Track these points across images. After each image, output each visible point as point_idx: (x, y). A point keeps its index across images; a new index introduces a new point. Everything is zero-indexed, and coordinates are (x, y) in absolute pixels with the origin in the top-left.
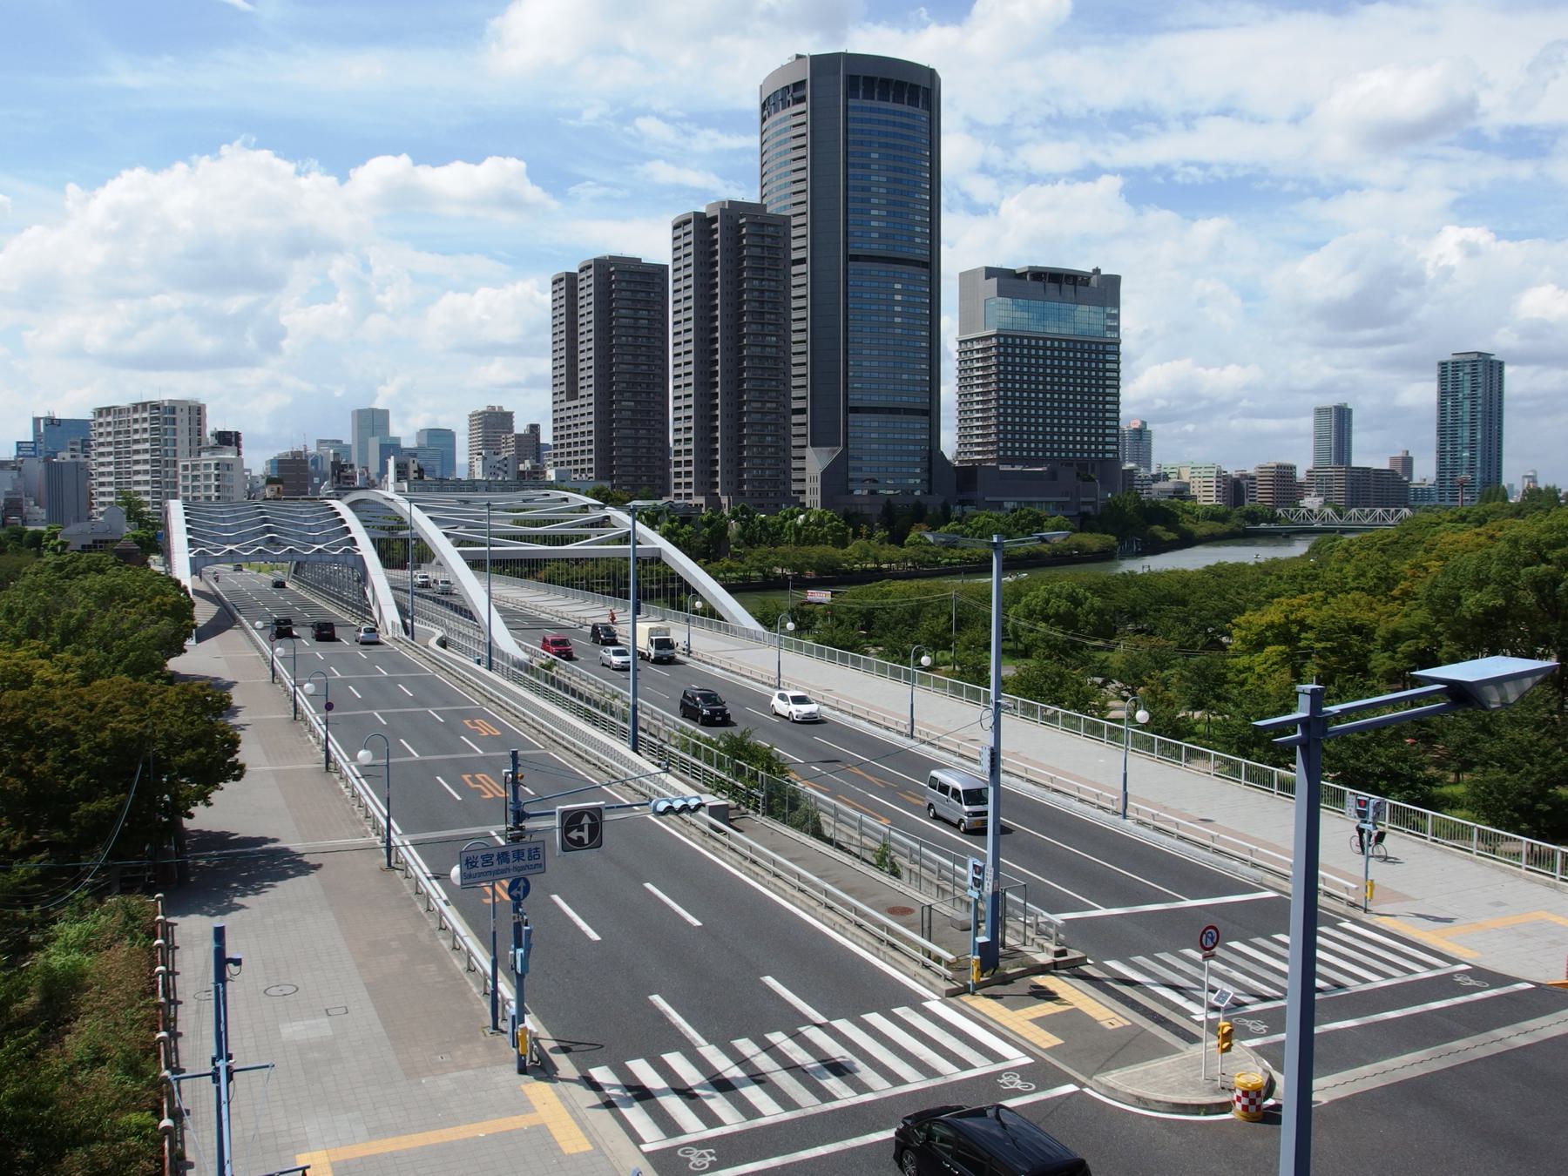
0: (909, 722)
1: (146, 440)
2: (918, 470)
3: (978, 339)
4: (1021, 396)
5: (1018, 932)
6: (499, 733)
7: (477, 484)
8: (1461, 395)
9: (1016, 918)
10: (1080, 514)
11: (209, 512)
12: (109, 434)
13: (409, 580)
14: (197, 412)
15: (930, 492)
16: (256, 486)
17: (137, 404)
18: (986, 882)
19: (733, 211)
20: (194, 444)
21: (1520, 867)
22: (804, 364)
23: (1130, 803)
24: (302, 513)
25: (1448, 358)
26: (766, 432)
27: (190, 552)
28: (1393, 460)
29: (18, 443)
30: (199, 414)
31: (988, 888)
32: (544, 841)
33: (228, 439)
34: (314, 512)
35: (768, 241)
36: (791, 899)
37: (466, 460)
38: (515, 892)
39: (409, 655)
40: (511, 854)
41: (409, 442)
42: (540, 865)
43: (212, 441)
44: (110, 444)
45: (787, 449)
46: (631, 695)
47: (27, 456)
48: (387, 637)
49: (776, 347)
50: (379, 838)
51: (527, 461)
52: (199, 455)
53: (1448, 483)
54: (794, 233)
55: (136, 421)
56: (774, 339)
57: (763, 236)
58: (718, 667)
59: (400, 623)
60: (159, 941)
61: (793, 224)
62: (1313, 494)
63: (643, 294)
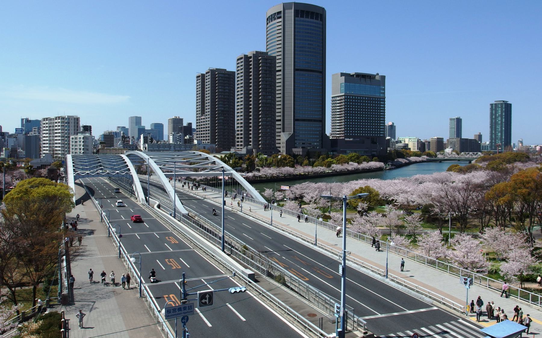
0: (315, 240)
1: (59, 129)
2: (318, 140)
3: (338, 96)
4: (355, 124)
5: (351, 325)
6: (178, 242)
7: (171, 145)
8: (497, 115)
9: (350, 318)
10: (372, 155)
11: (80, 159)
12: (47, 127)
13: (148, 179)
14: (77, 120)
15: (322, 148)
16: (96, 143)
17: (57, 117)
18: (341, 312)
19: (257, 54)
20: (76, 131)
21: (518, 298)
22: (280, 116)
23: (389, 273)
24: (112, 159)
25: (493, 102)
26: (268, 128)
27: (74, 174)
28: (475, 135)
29: (16, 129)
30: (78, 124)
31: (341, 314)
32: (193, 303)
33: (87, 129)
34: (116, 159)
35: (268, 65)
36: (275, 310)
37: (168, 136)
38: (183, 321)
39: (147, 210)
40: (182, 308)
41: (148, 127)
42: (192, 311)
43: (82, 129)
44: (47, 130)
45: (274, 134)
46: (222, 229)
47: (19, 133)
48: (140, 203)
49: (271, 100)
50: (137, 285)
51: (187, 136)
52: (77, 134)
53: (493, 144)
54: (277, 61)
55: (56, 123)
56: (270, 97)
57: (267, 63)
58: (251, 216)
59: (144, 199)
60: (62, 330)
61: (277, 58)
62: (449, 147)
63: (227, 81)
